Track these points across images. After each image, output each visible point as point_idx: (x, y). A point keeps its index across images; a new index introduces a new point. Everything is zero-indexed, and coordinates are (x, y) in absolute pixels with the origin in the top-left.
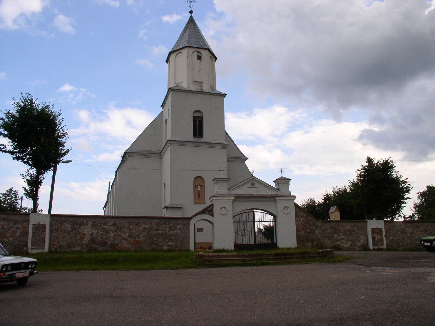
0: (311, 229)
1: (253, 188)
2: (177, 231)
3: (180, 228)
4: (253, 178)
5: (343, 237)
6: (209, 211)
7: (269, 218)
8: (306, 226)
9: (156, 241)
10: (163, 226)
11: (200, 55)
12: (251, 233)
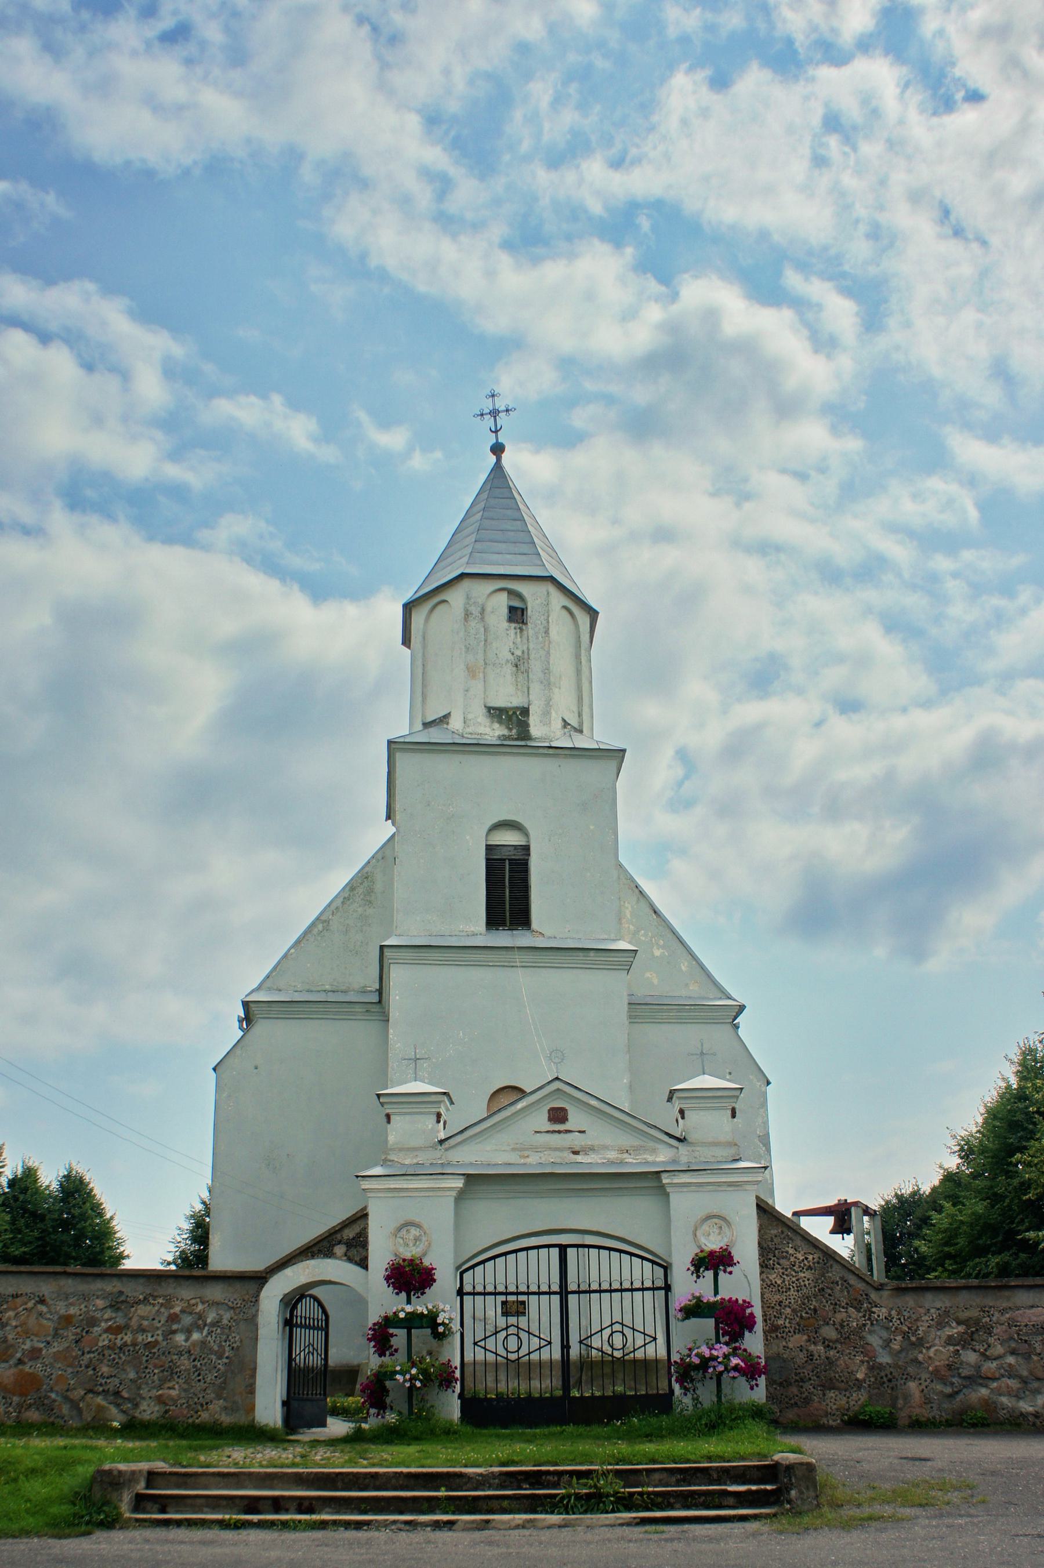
0: (842, 1326)
1: (559, 1132)
2: (205, 1332)
3: (216, 1324)
4: (558, 1089)
5: (1010, 1364)
6: (350, 1244)
7: (637, 1274)
8: (815, 1310)
9: (108, 1381)
10: (143, 1310)
11: (517, 604)
12: (475, 1344)
